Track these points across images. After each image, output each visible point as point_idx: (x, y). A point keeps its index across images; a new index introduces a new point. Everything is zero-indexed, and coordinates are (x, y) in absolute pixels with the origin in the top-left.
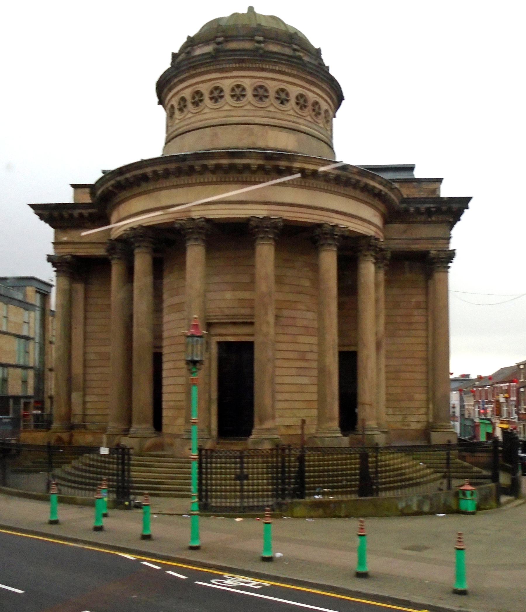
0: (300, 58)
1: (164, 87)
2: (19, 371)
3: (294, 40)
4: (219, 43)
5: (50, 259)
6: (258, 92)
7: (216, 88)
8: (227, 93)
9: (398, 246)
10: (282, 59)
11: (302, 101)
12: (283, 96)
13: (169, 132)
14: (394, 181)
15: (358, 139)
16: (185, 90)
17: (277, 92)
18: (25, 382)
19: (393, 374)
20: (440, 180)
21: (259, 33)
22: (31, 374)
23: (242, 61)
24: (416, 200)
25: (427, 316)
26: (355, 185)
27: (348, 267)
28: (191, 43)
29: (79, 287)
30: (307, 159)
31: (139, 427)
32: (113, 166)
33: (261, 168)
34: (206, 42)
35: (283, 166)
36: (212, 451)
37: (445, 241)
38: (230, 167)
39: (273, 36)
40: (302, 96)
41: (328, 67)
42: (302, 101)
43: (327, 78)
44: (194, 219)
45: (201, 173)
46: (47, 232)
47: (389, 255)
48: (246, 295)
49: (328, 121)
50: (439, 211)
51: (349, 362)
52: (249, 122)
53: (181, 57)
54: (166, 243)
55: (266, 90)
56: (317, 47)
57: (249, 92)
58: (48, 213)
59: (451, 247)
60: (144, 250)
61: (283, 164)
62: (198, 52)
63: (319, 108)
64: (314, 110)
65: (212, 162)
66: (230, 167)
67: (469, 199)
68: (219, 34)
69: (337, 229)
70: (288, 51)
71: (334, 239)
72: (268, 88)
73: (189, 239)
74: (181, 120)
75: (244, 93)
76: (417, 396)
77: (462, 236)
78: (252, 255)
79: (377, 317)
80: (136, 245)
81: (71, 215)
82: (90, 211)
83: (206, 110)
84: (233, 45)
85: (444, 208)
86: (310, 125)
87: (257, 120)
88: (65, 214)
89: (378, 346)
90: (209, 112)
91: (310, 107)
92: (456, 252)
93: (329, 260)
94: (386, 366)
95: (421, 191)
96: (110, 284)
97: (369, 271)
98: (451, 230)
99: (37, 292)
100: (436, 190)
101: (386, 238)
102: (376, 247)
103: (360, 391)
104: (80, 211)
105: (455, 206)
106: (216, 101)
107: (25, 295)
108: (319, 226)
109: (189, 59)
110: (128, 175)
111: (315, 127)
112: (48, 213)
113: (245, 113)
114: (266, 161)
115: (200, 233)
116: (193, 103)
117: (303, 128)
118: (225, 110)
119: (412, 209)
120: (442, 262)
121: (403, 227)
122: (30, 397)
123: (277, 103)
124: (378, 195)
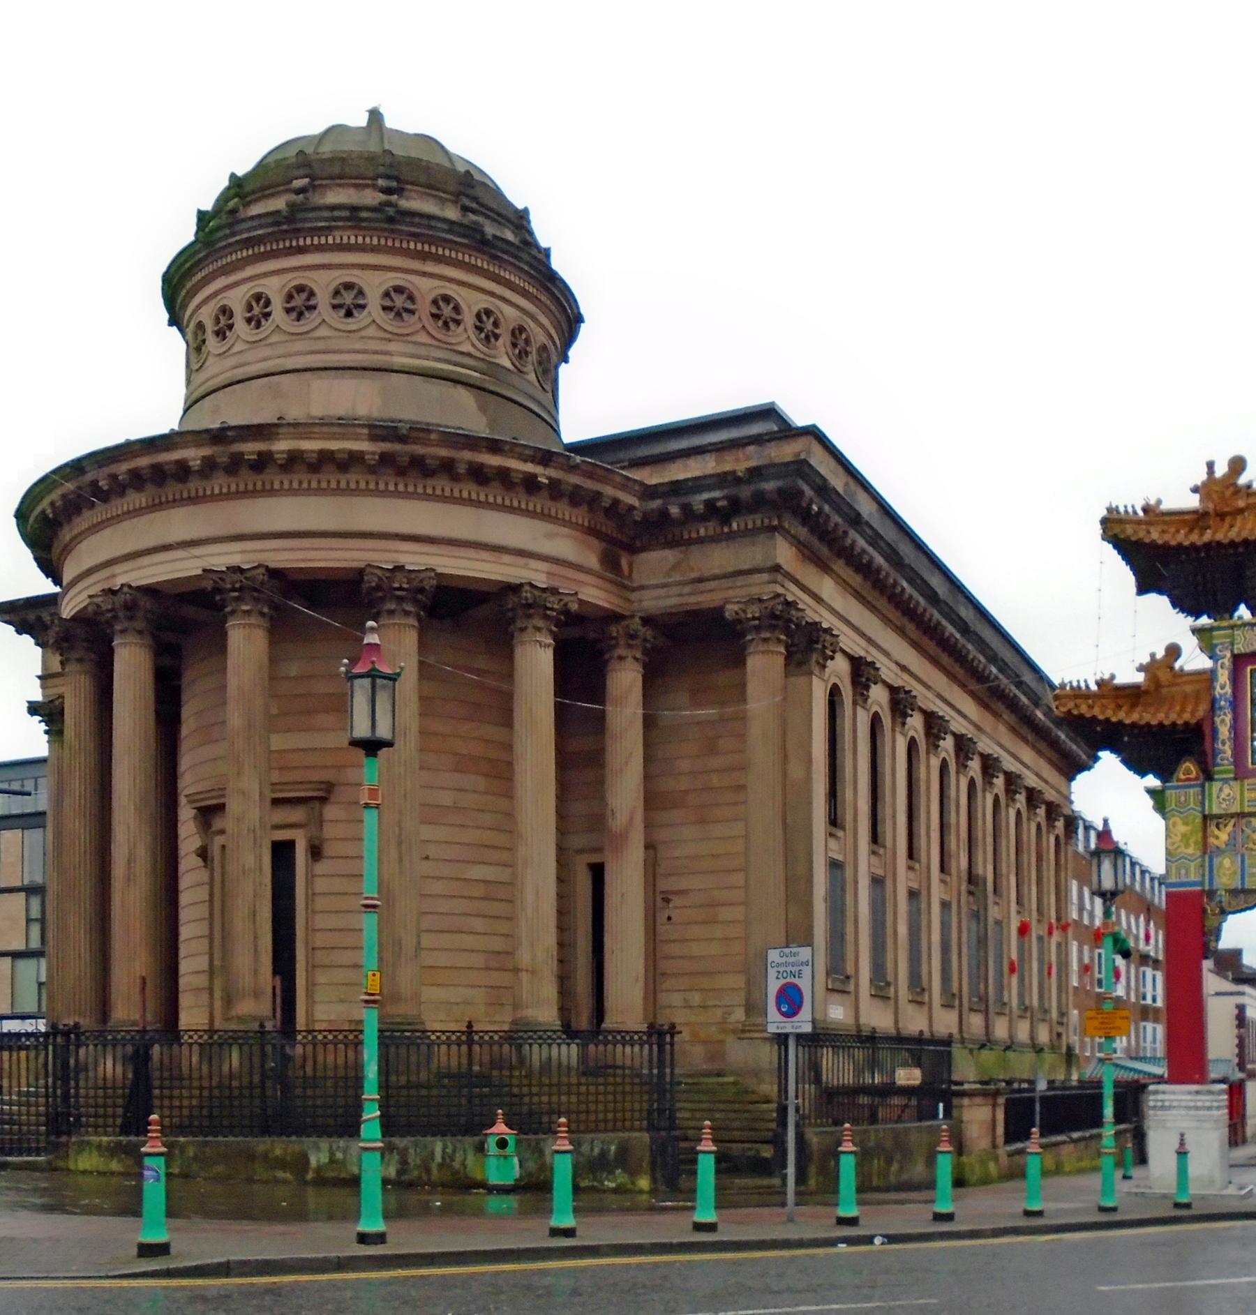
1: (179, 286)
3: (470, 188)
6: (392, 300)
27: (580, 673)
40: (488, 313)
41: (547, 252)
42: (486, 325)
45: (455, 478)
52: (273, 370)
56: (520, 206)
63: (527, 341)
65: (122, 468)
71: (546, 617)
72: (416, 294)
73: (233, 612)
75: (361, 302)
87: (290, 363)
93: (536, 661)
108: (515, 588)
114: (215, 448)
118: (319, 338)
123: (336, 318)
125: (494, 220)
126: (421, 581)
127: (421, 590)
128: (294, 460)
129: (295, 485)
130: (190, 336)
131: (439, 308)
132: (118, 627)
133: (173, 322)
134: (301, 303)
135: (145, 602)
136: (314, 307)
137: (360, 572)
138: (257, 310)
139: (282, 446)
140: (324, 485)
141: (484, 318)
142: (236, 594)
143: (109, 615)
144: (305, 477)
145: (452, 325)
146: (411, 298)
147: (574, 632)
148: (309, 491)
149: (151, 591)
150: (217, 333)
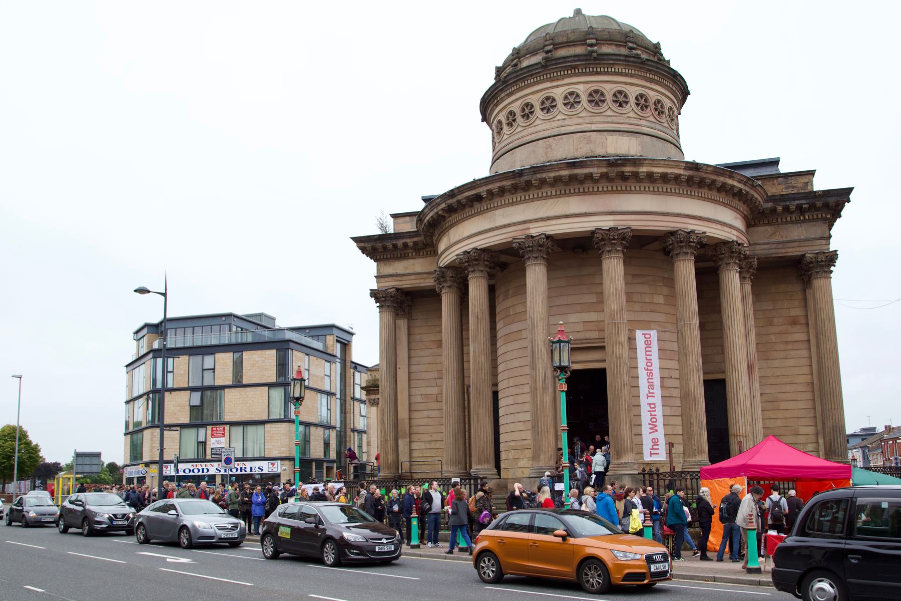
0: (637, 57)
1: (488, 104)
2: (320, 431)
4: (547, 52)
5: (374, 294)
7: (527, 105)
8: (560, 102)
9: (766, 252)
10: (617, 60)
11: (642, 102)
12: (621, 98)
13: (497, 150)
14: (757, 178)
15: (708, 136)
16: (514, 102)
17: (615, 95)
18: (327, 445)
19: (770, 404)
20: (811, 173)
21: (591, 36)
22: (333, 434)
23: (575, 67)
24: (782, 198)
25: (808, 332)
26: (711, 185)
28: (518, 54)
29: (403, 323)
30: (654, 162)
31: (479, 467)
32: (440, 188)
33: (604, 176)
34: (533, 52)
37: (824, 242)
38: (573, 178)
39: (607, 37)
40: (642, 96)
41: (668, 62)
42: (642, 102)
43: (668, 73)
44: (532, 237)
45: (539, 187)
46: (370, 266)
47: (755, 263)
48: (593, 316)
49: (673, 119)
50: (813, 207)
51: (716, 392)
53: (508, 70)
54: (502, 265)
55: (602, 94)
56: (655, 42)
57: (584, 99)
58: (371, 246)
59: (832, 248)
60: (478, 274)
61: (628, 169)
62: (525, 63)
64: (656, 109)
66: (573, 178)
67: (850, 190)
68: (548, 42)
69: (693, 236)
70: (623, 51)
71: (691, 247)
73: (529, 258)
74: (511, 135)
76: (803, 430)
77: (842, 235)
78: (600, 272)
79: (747, 335)
80: (470, 269)
81: (395, 246)
82: (415, 239)
83: (538, 122)
84: (562, 53)
85: (819, 204)
86: (653, 125)
87: (594, 127)
88: (389, 245)
89: (750, 368)
90: (541, 124)
91: (653, 106)
93: (686, 271)
94: (761, 394)
95: (788, 187)
96: (440, 317)
97: (733, 283)
98: (830, 229)
99: (337, 341)
100: (810, 183)
101: (750, 244)
102: (740, 253)
103: (731, 421)
104: (404, 241)
105: (832, 200)
107: (325, 345)
108: (673, 233)
109: (516, 72)
110: (459, 197)
111: (658, 127)
112: (371, 246)
113: (580, 121)
115: (540, 251)
116: (523, 116)
117: (646, 130)
119: (780, 208)
120: (822, 266)
121: (769, 229)
122: (333, 461)
123: (615, 107)
124: (738, 195)
128: (650, 177)
130: (494, 127)
134: (572, 100)
137: (593, 233)
138: (527, 111)
139: (644, 169)
141: (618, 95)
144: (510, 197)
147: (702, 251)
150: (508, 124)
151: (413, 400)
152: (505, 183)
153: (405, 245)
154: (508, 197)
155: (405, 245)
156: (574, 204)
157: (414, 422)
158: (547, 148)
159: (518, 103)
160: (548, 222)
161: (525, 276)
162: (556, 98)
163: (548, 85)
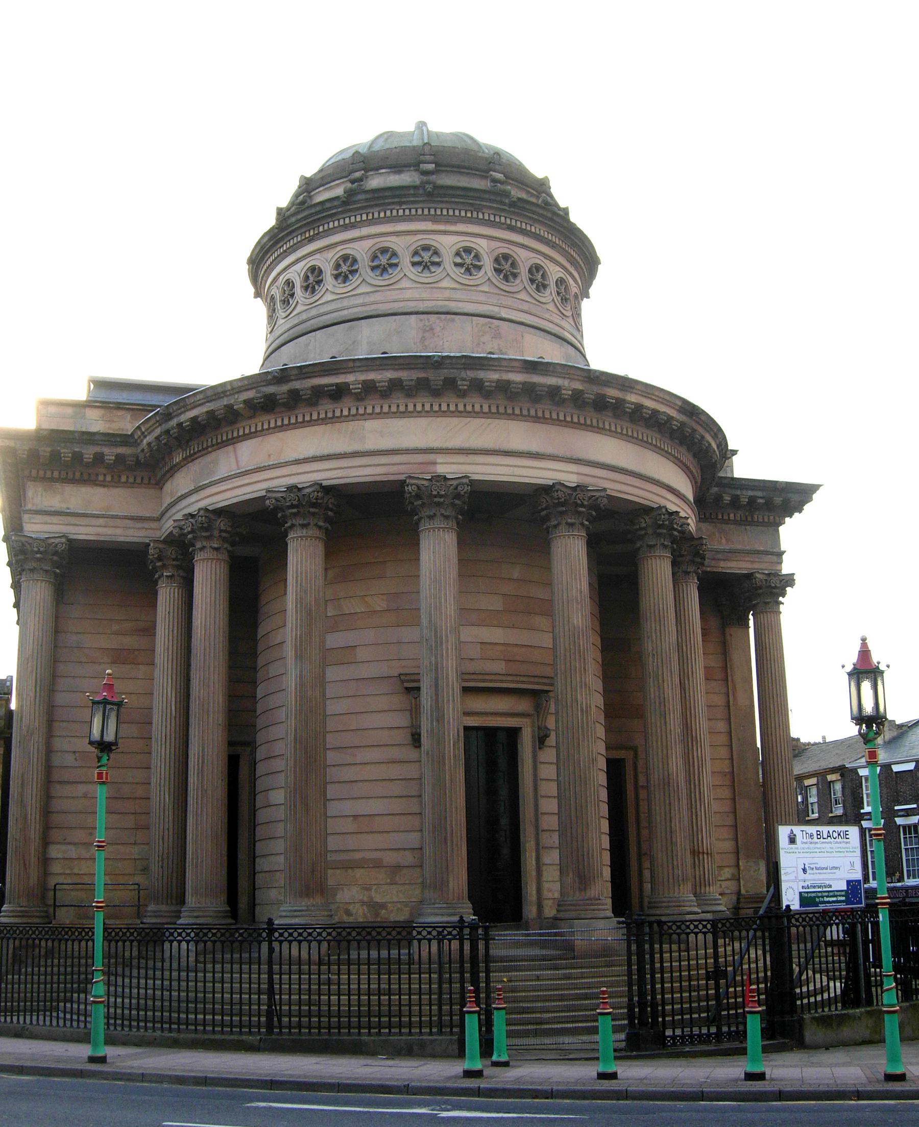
4: (353, 182)
6: (420, 256)
16: (321, 253)
34: (397, 167)
35: (612, 398)
36: (555, 918)
37: (775, 558)
41: (566, 211)
44: (445, 478)
45: (462, 394)
61: (612, 392)
67: (813, 488)
73: (293, 526)
82: (121, 450)
83: (405, 284)
90: (408, 287)
91: (552, 287)
92: (795, 577)
93: (571, 554)
106: (346, 279)
108: (647, 510)
114: (587, 385)
119: (727, 498)
123: (412, 272)
125: (468, 174)
126: (456, 488)
127: (458, 496)
129: (419, 408)
131: (462, 258)
132: (198, 545)
133: (258, 294)
134: (346, 269)
135: (221, 524)
136: (396, 265)
137: (403, 483)
140: (394, 409)
141: (503, 262)
142: (295, 510)
143: (190, 536)
144: (402, 402)
145: (511, 278)
146: (436, 253)
148: (431, 413)
149: (220, 512)
151: (56, 760)
152: (403, 375)
153: (99, 458)
154: (399, 401)
155: (99, 458)
156: (517, 434)
157: (57, 805)
158: (425, 331)
159: (367, 244)
160: (472, 458)
161: (418, 544)
162: (442, 251)
163: (428, 226)
